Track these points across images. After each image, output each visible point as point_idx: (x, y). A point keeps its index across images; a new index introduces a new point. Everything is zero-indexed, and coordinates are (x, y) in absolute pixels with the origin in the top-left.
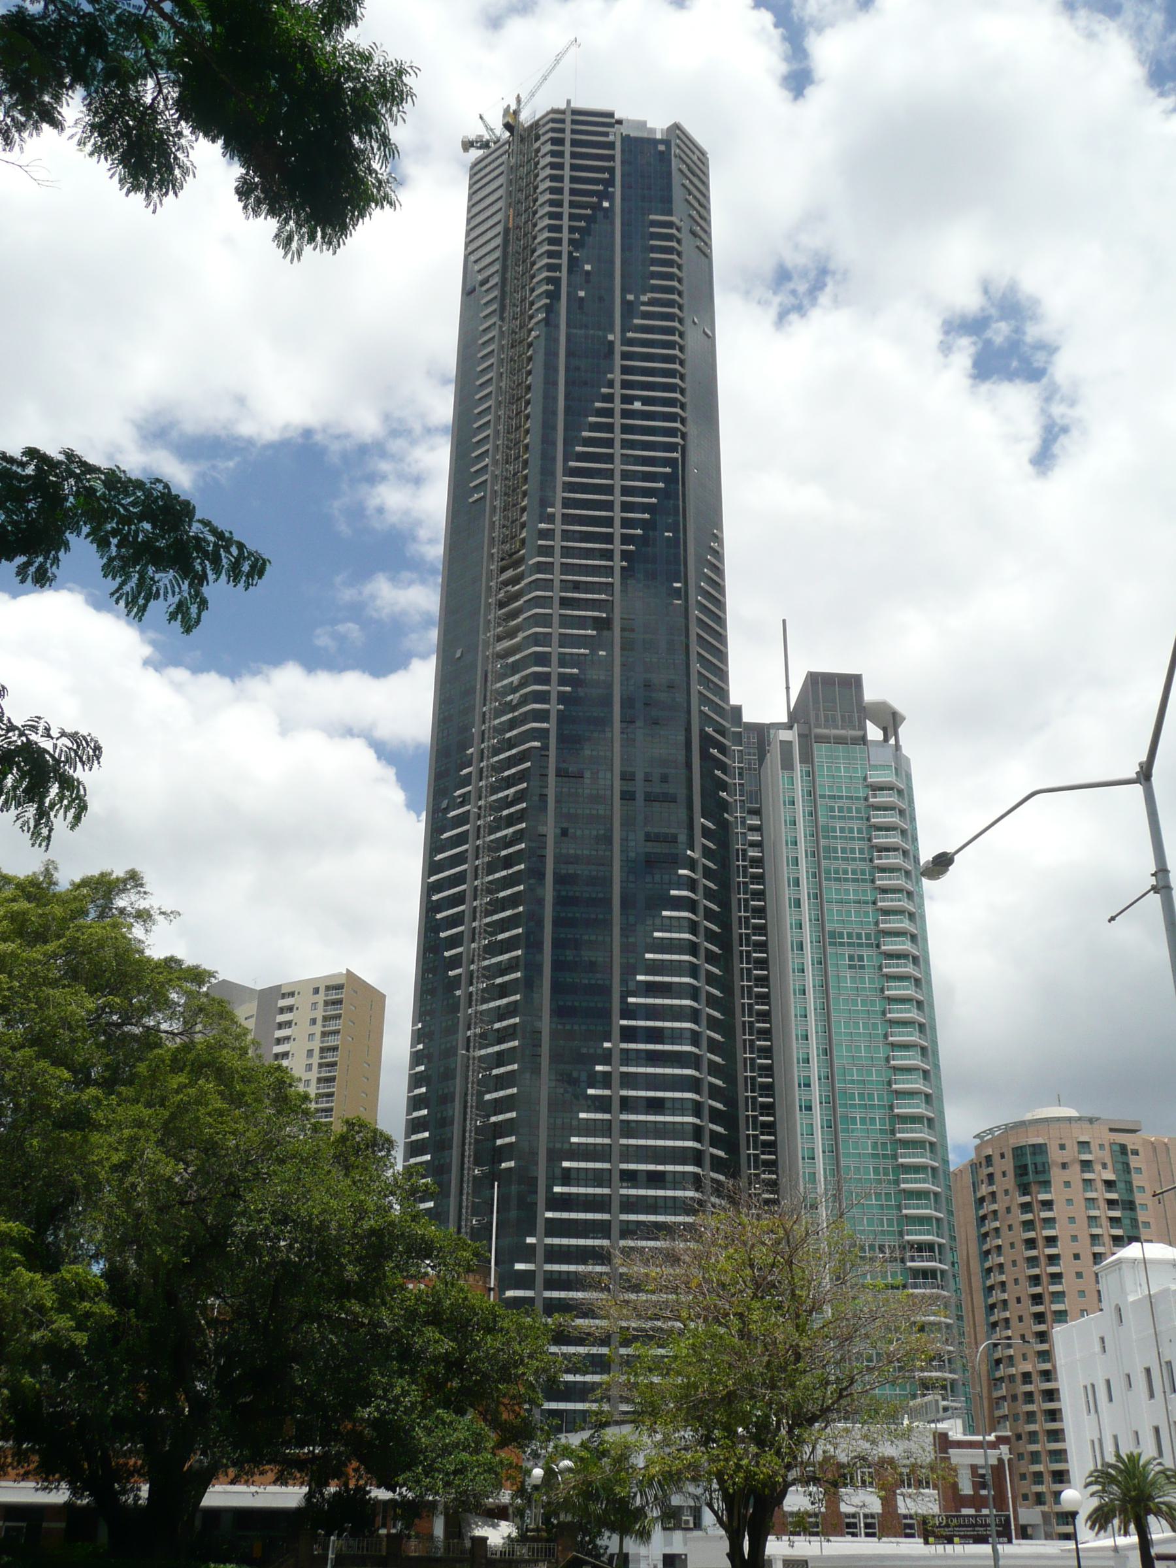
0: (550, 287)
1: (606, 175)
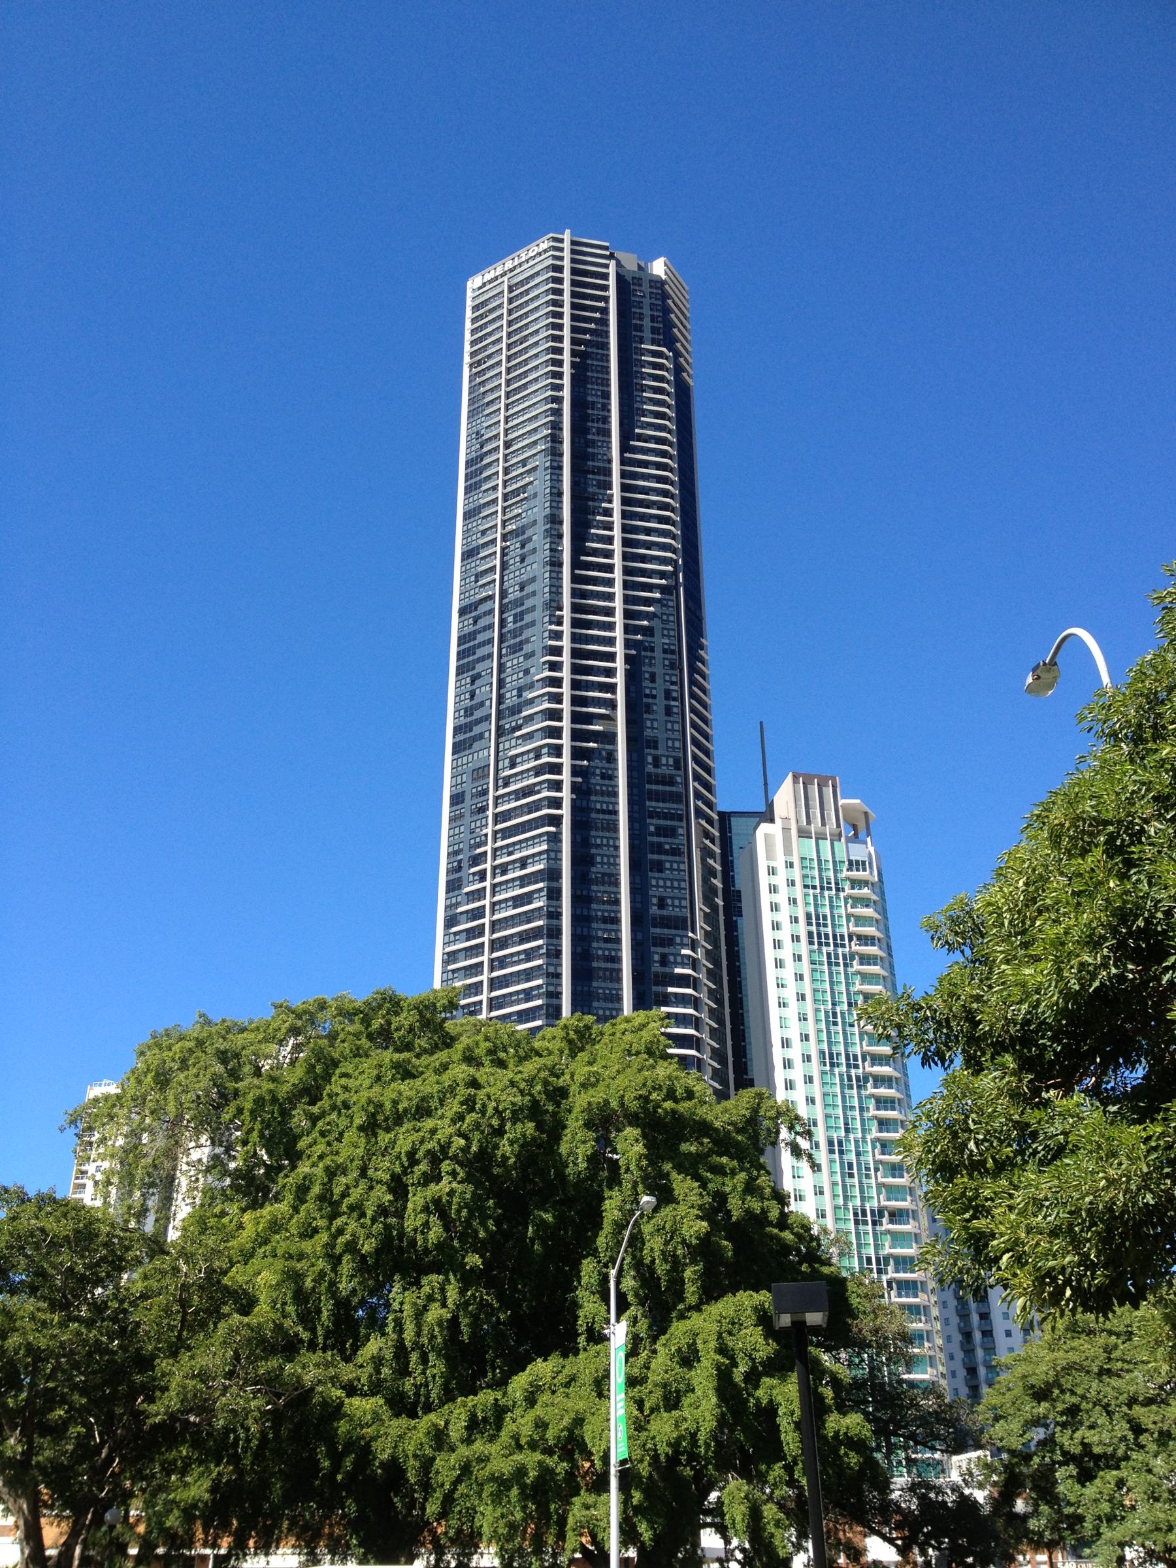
0: (554, 406)
1: (603, 304)
